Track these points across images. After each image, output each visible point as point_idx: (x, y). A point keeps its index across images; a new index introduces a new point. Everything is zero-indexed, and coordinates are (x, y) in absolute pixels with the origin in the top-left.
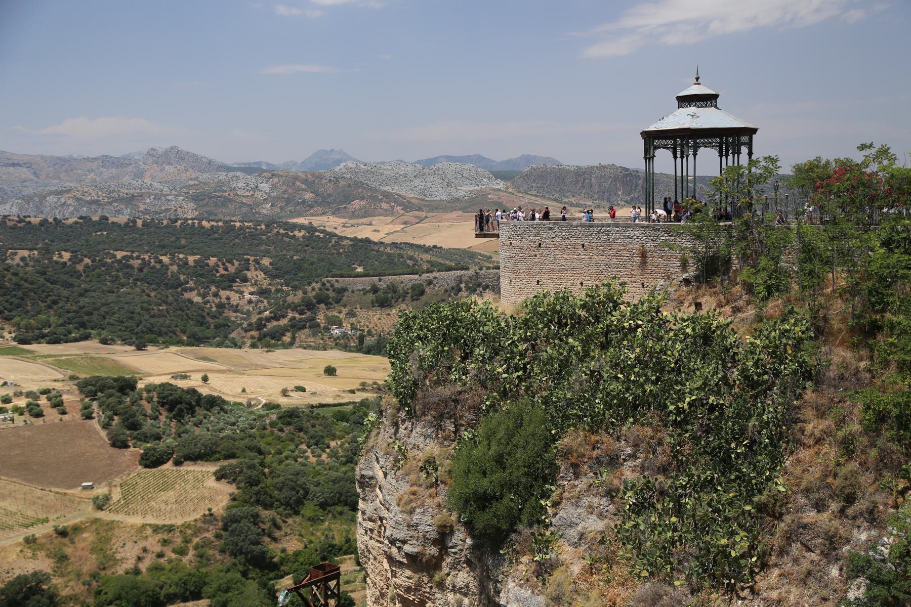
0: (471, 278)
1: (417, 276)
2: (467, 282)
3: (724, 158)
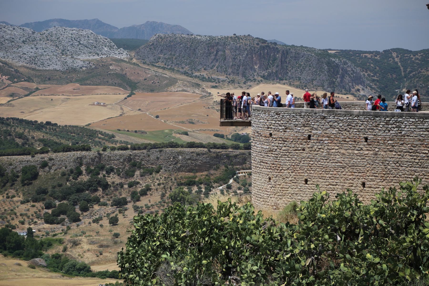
0: (93, 160)
1: (29, 157)
2: (88, 165)
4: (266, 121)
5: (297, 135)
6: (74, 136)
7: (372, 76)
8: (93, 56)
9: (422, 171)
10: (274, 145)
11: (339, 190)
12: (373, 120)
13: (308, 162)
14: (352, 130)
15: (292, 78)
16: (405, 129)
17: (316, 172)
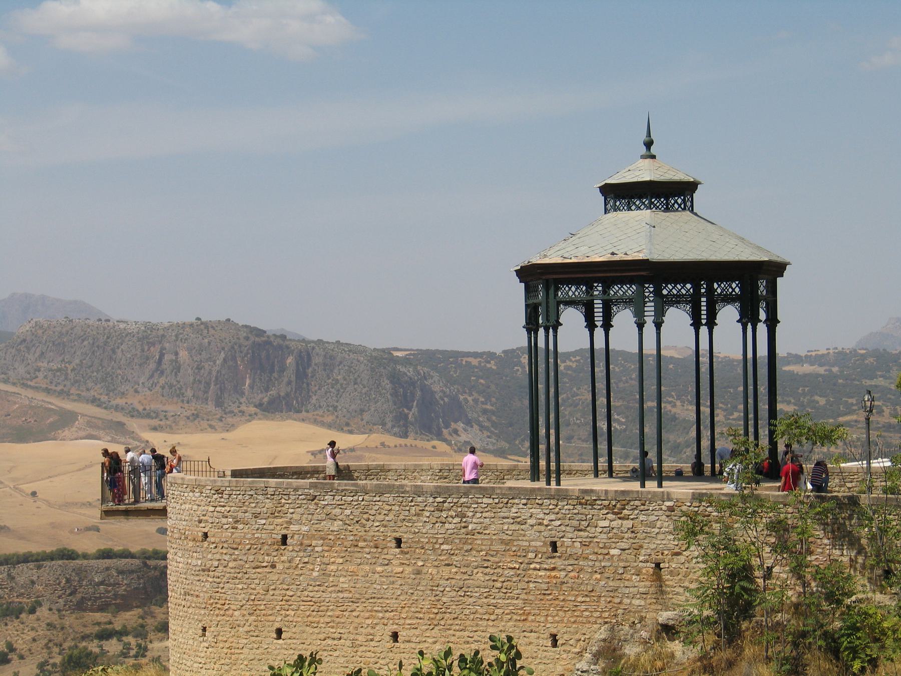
3: (704, 330)
4: (195, 507)
5: (259, 535)
7: (483, 403)
9: (508, 605)
10: (212, 557)
11: (345, 649)
12: (412, 501)
13: (284, 592)
14: (369, 523)
15: (320, 407)
16: (474, 520)
17: (300, 612)
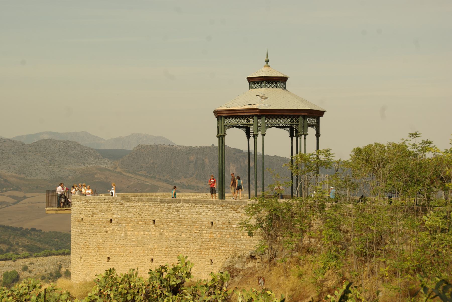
6: (57, 242)
8: (79, 165)
14: (143, 215)
